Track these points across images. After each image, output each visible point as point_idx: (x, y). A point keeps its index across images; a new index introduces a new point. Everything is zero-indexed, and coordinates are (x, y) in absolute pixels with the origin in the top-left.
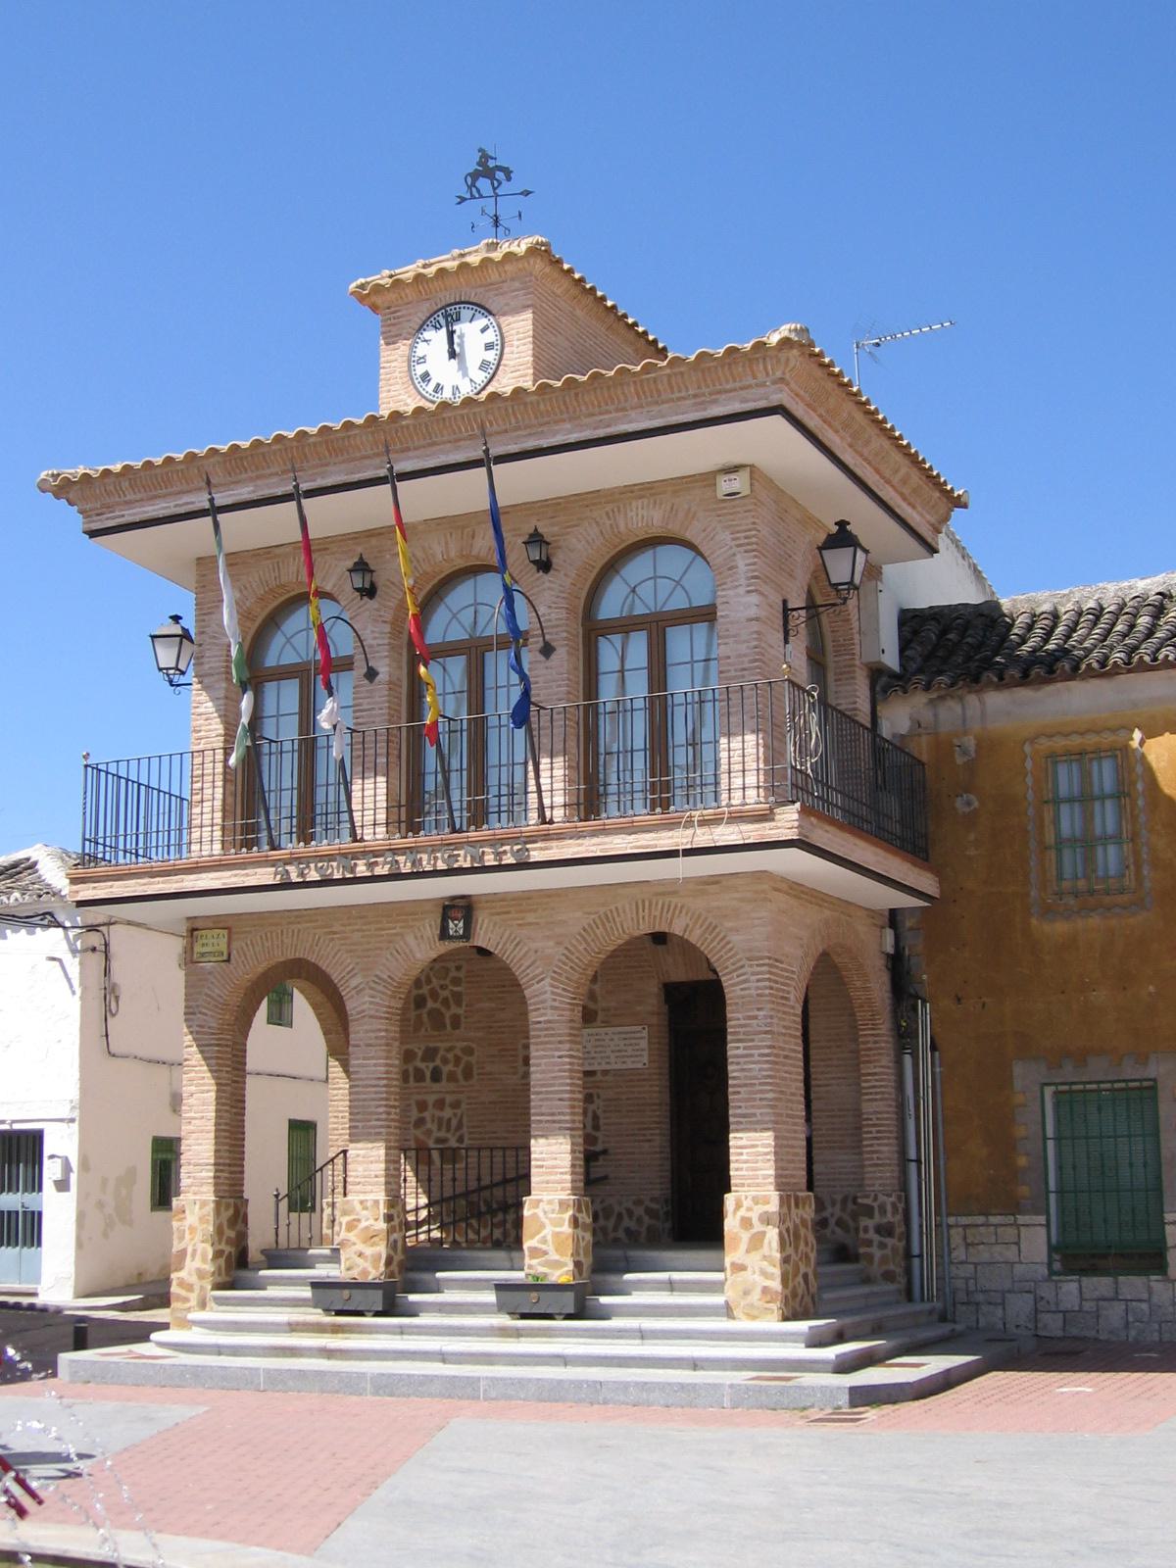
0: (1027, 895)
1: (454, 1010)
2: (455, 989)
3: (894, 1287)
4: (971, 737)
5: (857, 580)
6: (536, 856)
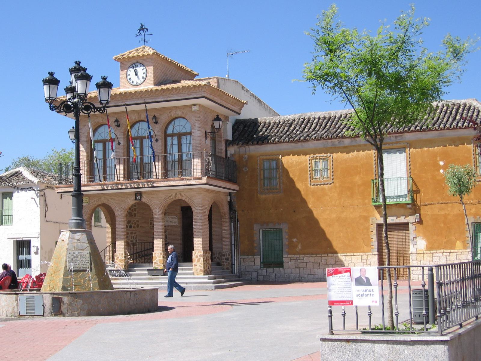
0: (258, 189)
1: (135, 212)
2: (135, 208)
3: (226, 269)
4: (247, 155)
5: (220, 127)
6: (155, 185)
